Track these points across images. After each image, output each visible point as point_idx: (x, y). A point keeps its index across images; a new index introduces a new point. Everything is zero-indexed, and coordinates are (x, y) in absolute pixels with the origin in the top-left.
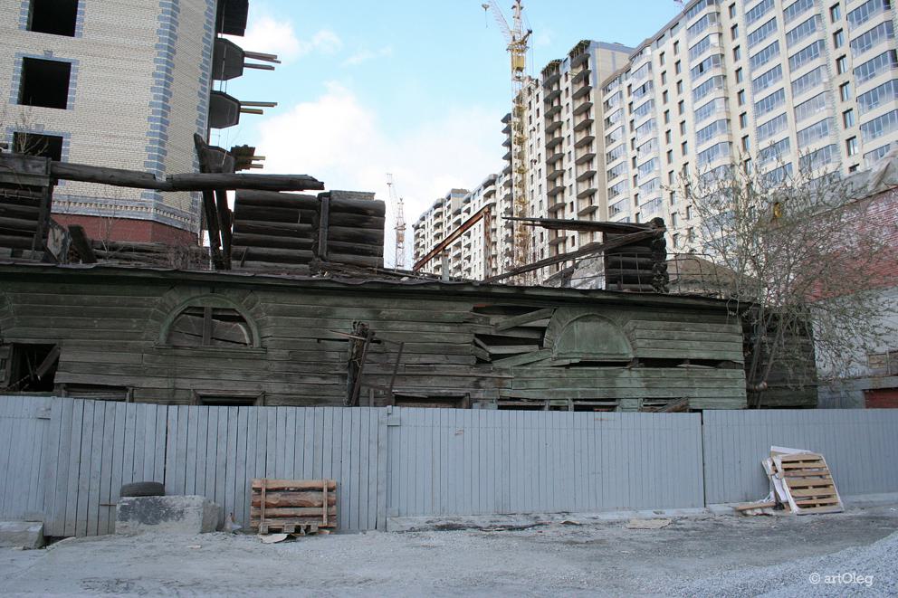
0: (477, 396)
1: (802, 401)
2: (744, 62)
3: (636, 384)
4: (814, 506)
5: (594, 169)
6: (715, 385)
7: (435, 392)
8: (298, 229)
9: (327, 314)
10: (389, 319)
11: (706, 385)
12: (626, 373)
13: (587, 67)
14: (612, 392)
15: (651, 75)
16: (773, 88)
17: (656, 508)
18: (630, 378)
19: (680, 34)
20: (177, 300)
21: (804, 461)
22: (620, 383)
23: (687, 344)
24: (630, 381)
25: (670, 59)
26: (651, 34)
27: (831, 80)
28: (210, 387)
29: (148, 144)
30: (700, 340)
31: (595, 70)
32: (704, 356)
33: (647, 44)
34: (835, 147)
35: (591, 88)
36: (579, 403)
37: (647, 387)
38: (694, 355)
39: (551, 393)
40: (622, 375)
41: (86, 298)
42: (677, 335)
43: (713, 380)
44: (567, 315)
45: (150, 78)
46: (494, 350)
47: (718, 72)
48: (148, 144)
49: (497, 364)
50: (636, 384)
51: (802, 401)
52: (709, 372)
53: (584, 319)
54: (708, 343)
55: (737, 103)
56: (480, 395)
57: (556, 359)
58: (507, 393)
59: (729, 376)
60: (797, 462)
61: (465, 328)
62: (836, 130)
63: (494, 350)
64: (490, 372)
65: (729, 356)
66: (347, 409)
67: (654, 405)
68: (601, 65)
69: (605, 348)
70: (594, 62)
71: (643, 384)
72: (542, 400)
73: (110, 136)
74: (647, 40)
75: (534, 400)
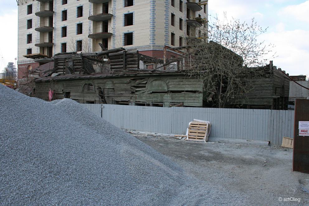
0: (131, 101)
1: (265, 103)
3: (169, 98)
4: (195, 138)
6: (192, 99)
7: (123, 100)
8: (121, 60)
9: (105, 83)
10: (115, 83)
11: (189, 99)
12: (166, 95)
14: (162, 100)
17: (155, 132)
18: (167, 97)
20: (83, 82)
21: (200, 125)
22: (164, 98)
23: (184, 86)
24: (167, 98)
28: (88, 99)
29: (150, 30)
30: (189, 85)
32: (189, 89)
36: (153, 103)
37: (172, 99)
38: (186, 89)
39: (147, 100)
40: (165, 96)
41: (73, 83)
42: (181, 83)
43: (192, 97)
44: (151, 79)
45: (150, 11)
46: (137, 89)
48: (150, 30)
49: (137, 93)
50: (169, 98)
51: (265, 103)
52: (191, 94)
53: (155, 80)
54: (191, 85)
56: (132, 101)
57: (148, 92)
58: (137, 100)
59: (197, 96)
60: (197, 124)
61: (129, 84)
63: (137, 89)
64: (134, 95)
65: (198, 89)
66: (112, 105)
67: (173, 104)
69: (160, 88)
71: (171, 98)
72: (145, 102)
73: (142, 29)
75: (143, 102)
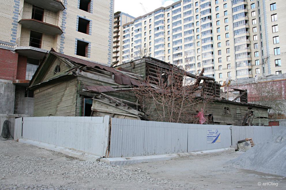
2: (170, 23)
5: (119, 45)
13: (119, 19)
15: (141, 32)
16: (179, 32)
19: (152, 17)
25: (148, 24)
26: (143, 14)
27: (195, 40)
31: (121, 21)
33: (140, 18)
34: (194, 50)
35: (120, 26)
47: (163, 31)
55: (167, 28)
62: (195, 46)
68: (123, 20)
70: (121, 18)
74: (140, 16)
